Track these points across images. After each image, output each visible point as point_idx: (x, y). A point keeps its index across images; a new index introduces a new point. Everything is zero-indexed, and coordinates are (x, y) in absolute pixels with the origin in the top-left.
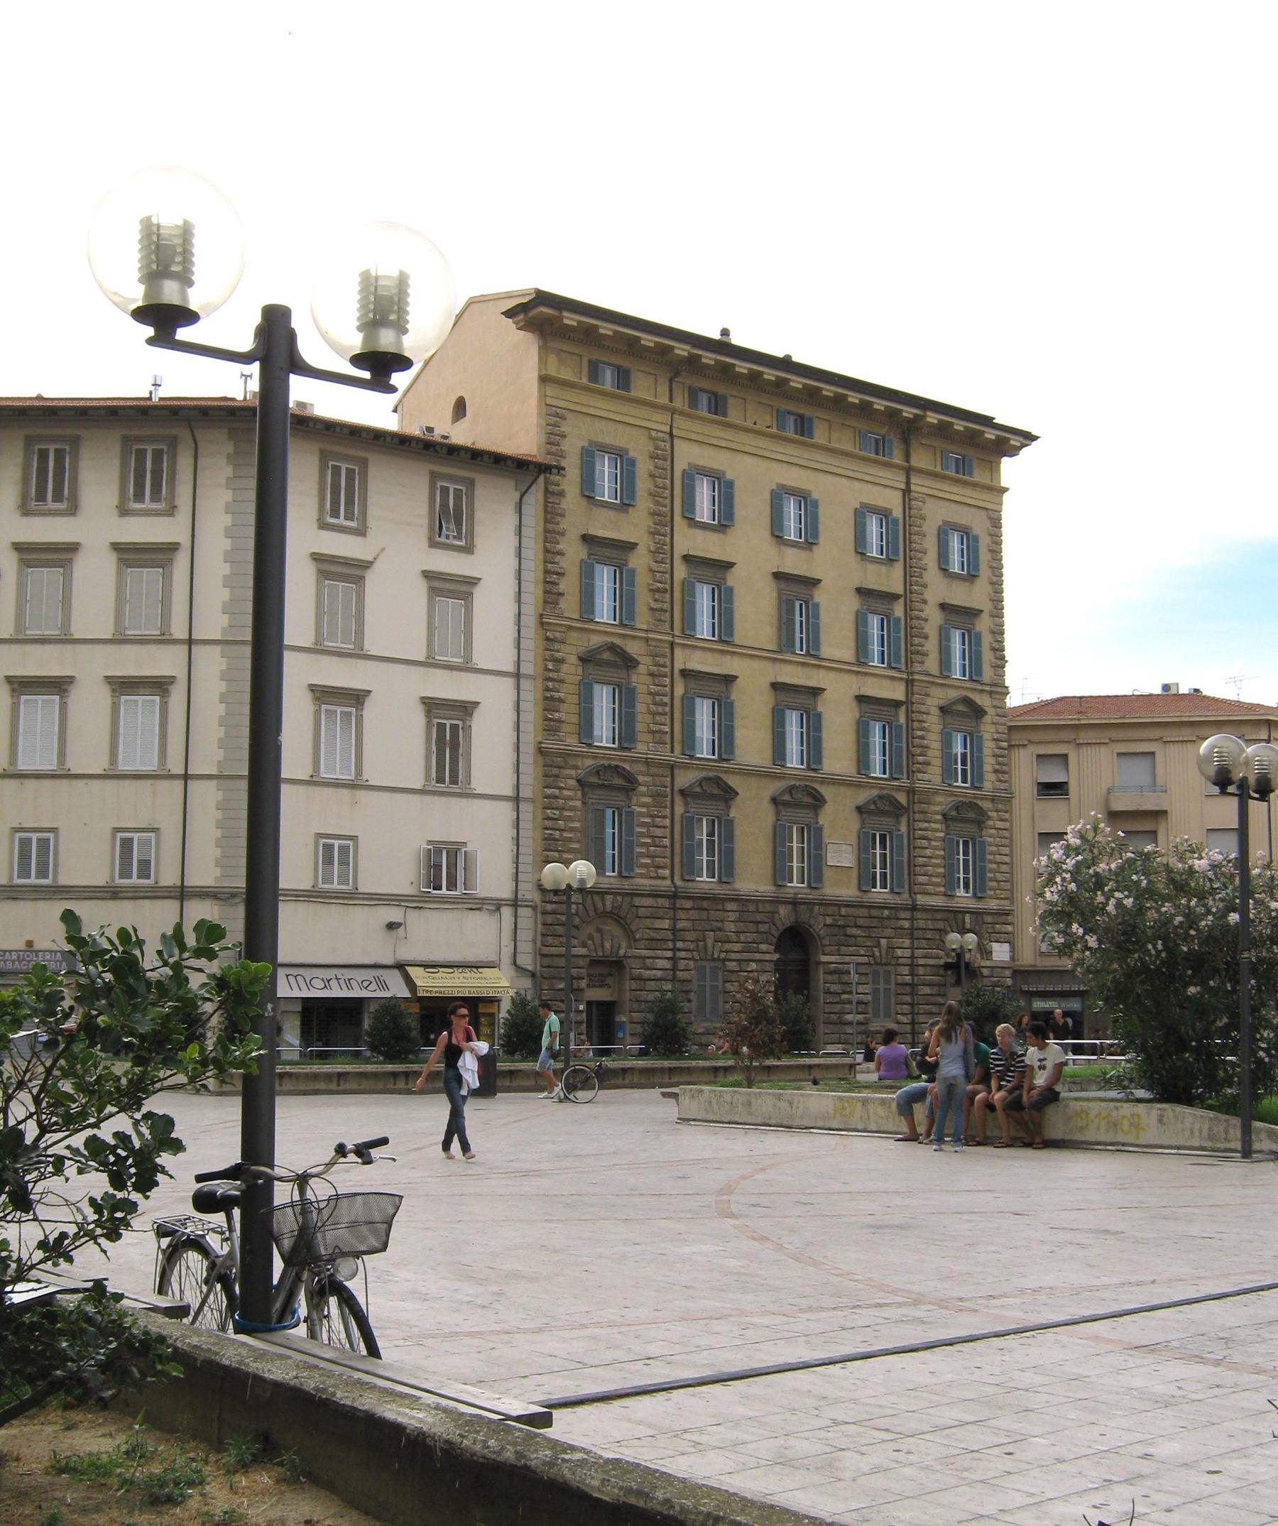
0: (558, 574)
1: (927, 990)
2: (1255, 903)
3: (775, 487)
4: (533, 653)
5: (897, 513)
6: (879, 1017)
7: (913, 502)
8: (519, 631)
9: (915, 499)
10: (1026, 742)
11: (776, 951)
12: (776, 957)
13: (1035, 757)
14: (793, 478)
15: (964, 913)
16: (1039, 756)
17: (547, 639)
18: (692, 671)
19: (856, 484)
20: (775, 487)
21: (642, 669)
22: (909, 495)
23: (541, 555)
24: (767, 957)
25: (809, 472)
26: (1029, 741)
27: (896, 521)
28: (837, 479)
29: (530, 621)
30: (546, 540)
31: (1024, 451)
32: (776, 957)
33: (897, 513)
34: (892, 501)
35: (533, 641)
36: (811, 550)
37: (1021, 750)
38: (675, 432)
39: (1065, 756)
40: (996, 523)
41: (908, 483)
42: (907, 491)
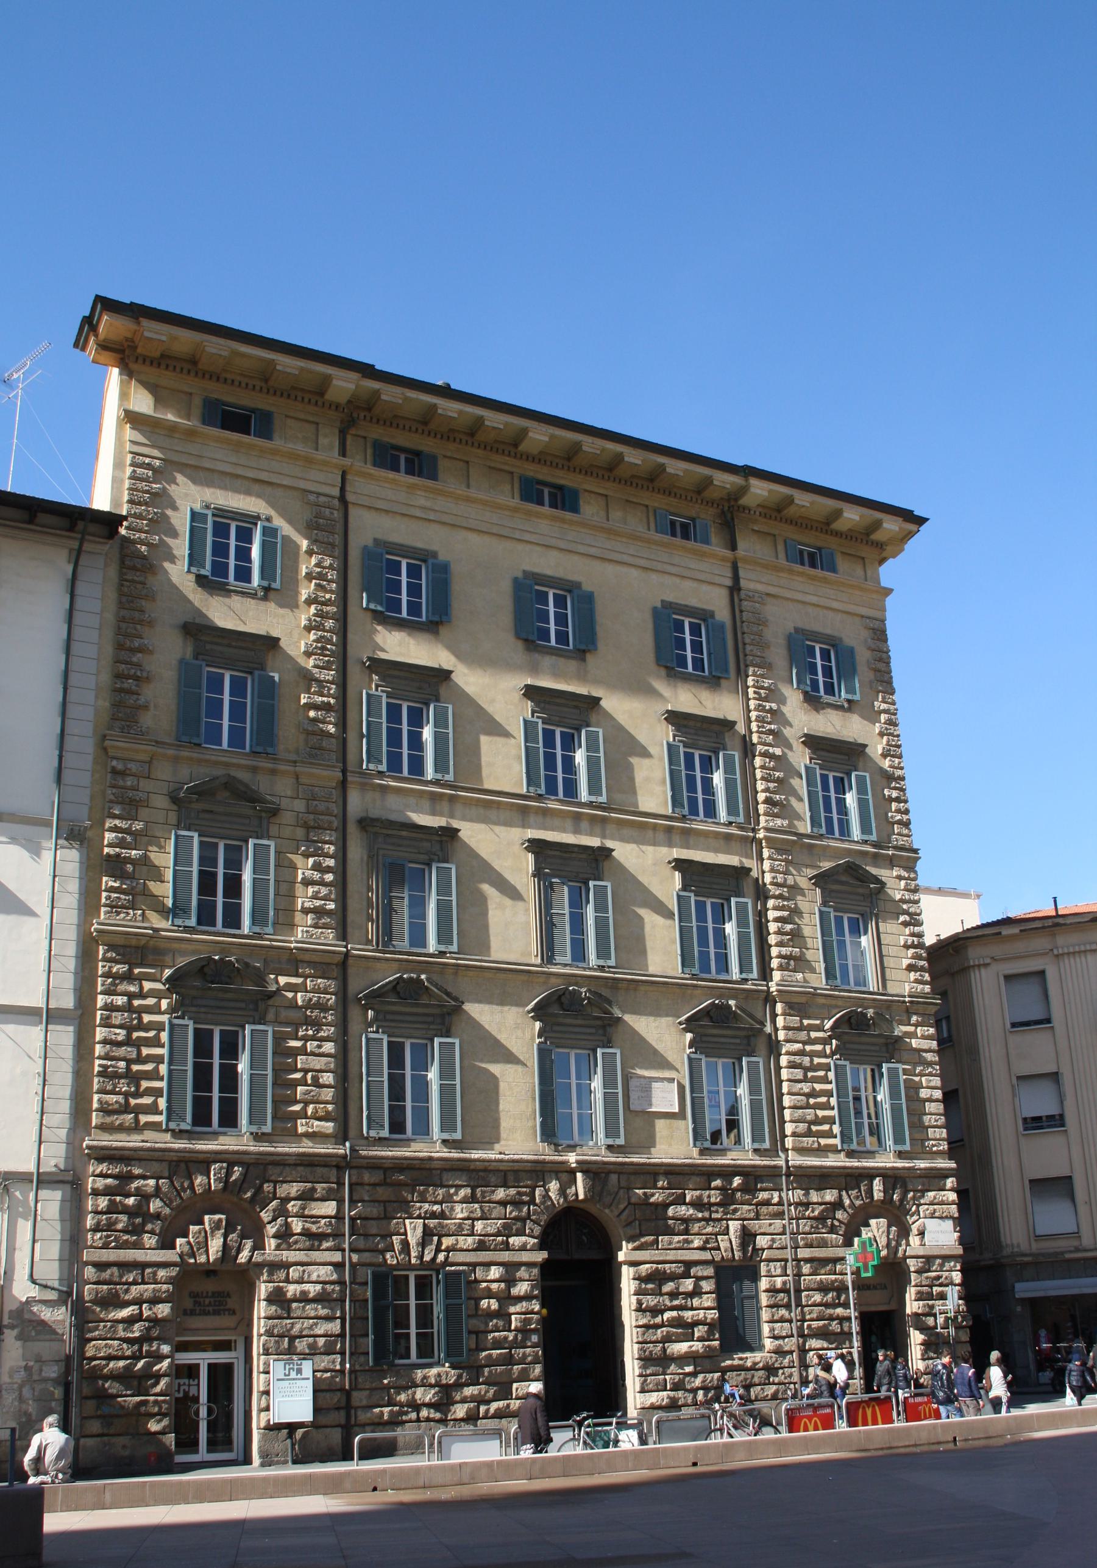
0: (137, 679)
1: (817, 1297)
2: (927, 1345)
3: (520, 575)
4: (88, 792)
5: (723, 614)
6: (352, 1459)
7: (745, 603)
8: (61, 757)
9: (749, 598)
10: (988, 961)
11: (541, 1247)
12: (541, 1256)
13: (1002, 979)
14: (549, 564)
15: (610, 1172)
16: (1008, 978)
17: (115, 772)
18: (377, 820)
19: (654, 576)
20: (520, 575)
21: (287, 818)
22: (738, 594)
23: (109, 649)
24: (526, 1257)
25: (576, 558)
26: (992, 958)
27: (722, 626)
28: (624, 569)
29: (83, 745)
30: (119, 631)
31: (911, 545)
32: (541, 1256)
33: (723, 614)
34: (716, 601)
35: (89, 774)
36: (584, 660)
37: (983, 970)
38: (350, 497)
39: (1042, 973)
40: (880, 634)
41: (736, 578)
42: (735, 589)
